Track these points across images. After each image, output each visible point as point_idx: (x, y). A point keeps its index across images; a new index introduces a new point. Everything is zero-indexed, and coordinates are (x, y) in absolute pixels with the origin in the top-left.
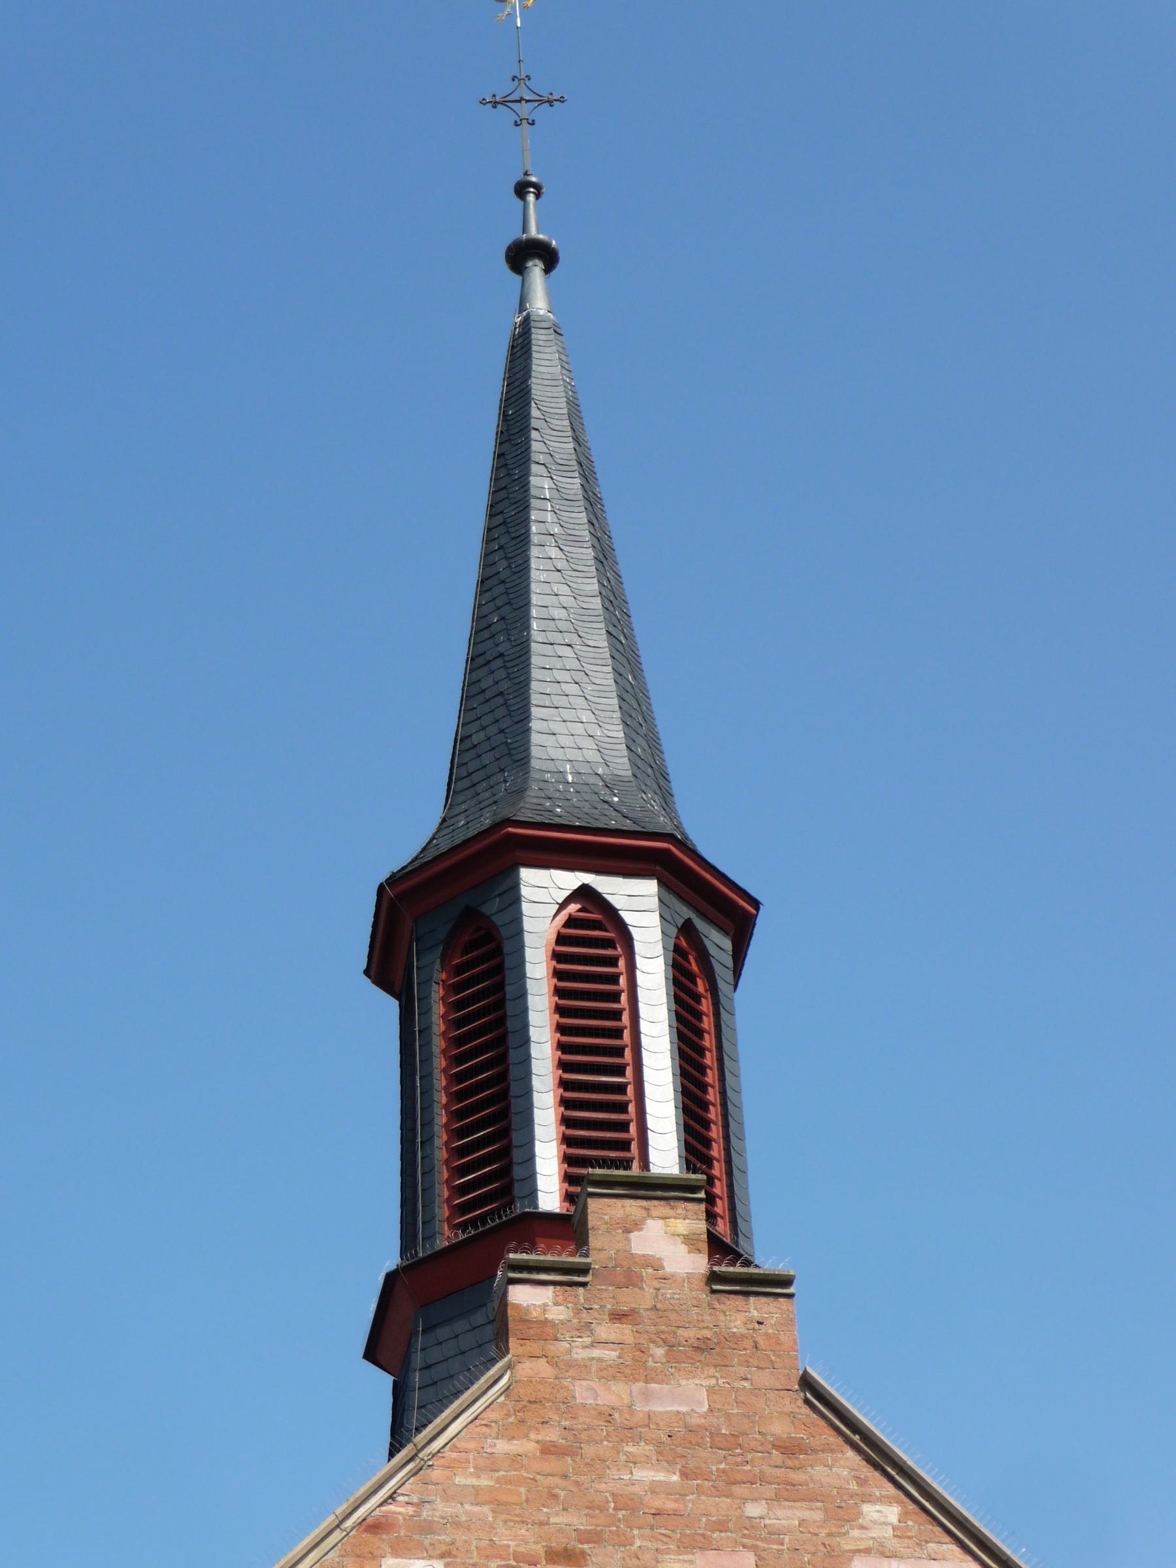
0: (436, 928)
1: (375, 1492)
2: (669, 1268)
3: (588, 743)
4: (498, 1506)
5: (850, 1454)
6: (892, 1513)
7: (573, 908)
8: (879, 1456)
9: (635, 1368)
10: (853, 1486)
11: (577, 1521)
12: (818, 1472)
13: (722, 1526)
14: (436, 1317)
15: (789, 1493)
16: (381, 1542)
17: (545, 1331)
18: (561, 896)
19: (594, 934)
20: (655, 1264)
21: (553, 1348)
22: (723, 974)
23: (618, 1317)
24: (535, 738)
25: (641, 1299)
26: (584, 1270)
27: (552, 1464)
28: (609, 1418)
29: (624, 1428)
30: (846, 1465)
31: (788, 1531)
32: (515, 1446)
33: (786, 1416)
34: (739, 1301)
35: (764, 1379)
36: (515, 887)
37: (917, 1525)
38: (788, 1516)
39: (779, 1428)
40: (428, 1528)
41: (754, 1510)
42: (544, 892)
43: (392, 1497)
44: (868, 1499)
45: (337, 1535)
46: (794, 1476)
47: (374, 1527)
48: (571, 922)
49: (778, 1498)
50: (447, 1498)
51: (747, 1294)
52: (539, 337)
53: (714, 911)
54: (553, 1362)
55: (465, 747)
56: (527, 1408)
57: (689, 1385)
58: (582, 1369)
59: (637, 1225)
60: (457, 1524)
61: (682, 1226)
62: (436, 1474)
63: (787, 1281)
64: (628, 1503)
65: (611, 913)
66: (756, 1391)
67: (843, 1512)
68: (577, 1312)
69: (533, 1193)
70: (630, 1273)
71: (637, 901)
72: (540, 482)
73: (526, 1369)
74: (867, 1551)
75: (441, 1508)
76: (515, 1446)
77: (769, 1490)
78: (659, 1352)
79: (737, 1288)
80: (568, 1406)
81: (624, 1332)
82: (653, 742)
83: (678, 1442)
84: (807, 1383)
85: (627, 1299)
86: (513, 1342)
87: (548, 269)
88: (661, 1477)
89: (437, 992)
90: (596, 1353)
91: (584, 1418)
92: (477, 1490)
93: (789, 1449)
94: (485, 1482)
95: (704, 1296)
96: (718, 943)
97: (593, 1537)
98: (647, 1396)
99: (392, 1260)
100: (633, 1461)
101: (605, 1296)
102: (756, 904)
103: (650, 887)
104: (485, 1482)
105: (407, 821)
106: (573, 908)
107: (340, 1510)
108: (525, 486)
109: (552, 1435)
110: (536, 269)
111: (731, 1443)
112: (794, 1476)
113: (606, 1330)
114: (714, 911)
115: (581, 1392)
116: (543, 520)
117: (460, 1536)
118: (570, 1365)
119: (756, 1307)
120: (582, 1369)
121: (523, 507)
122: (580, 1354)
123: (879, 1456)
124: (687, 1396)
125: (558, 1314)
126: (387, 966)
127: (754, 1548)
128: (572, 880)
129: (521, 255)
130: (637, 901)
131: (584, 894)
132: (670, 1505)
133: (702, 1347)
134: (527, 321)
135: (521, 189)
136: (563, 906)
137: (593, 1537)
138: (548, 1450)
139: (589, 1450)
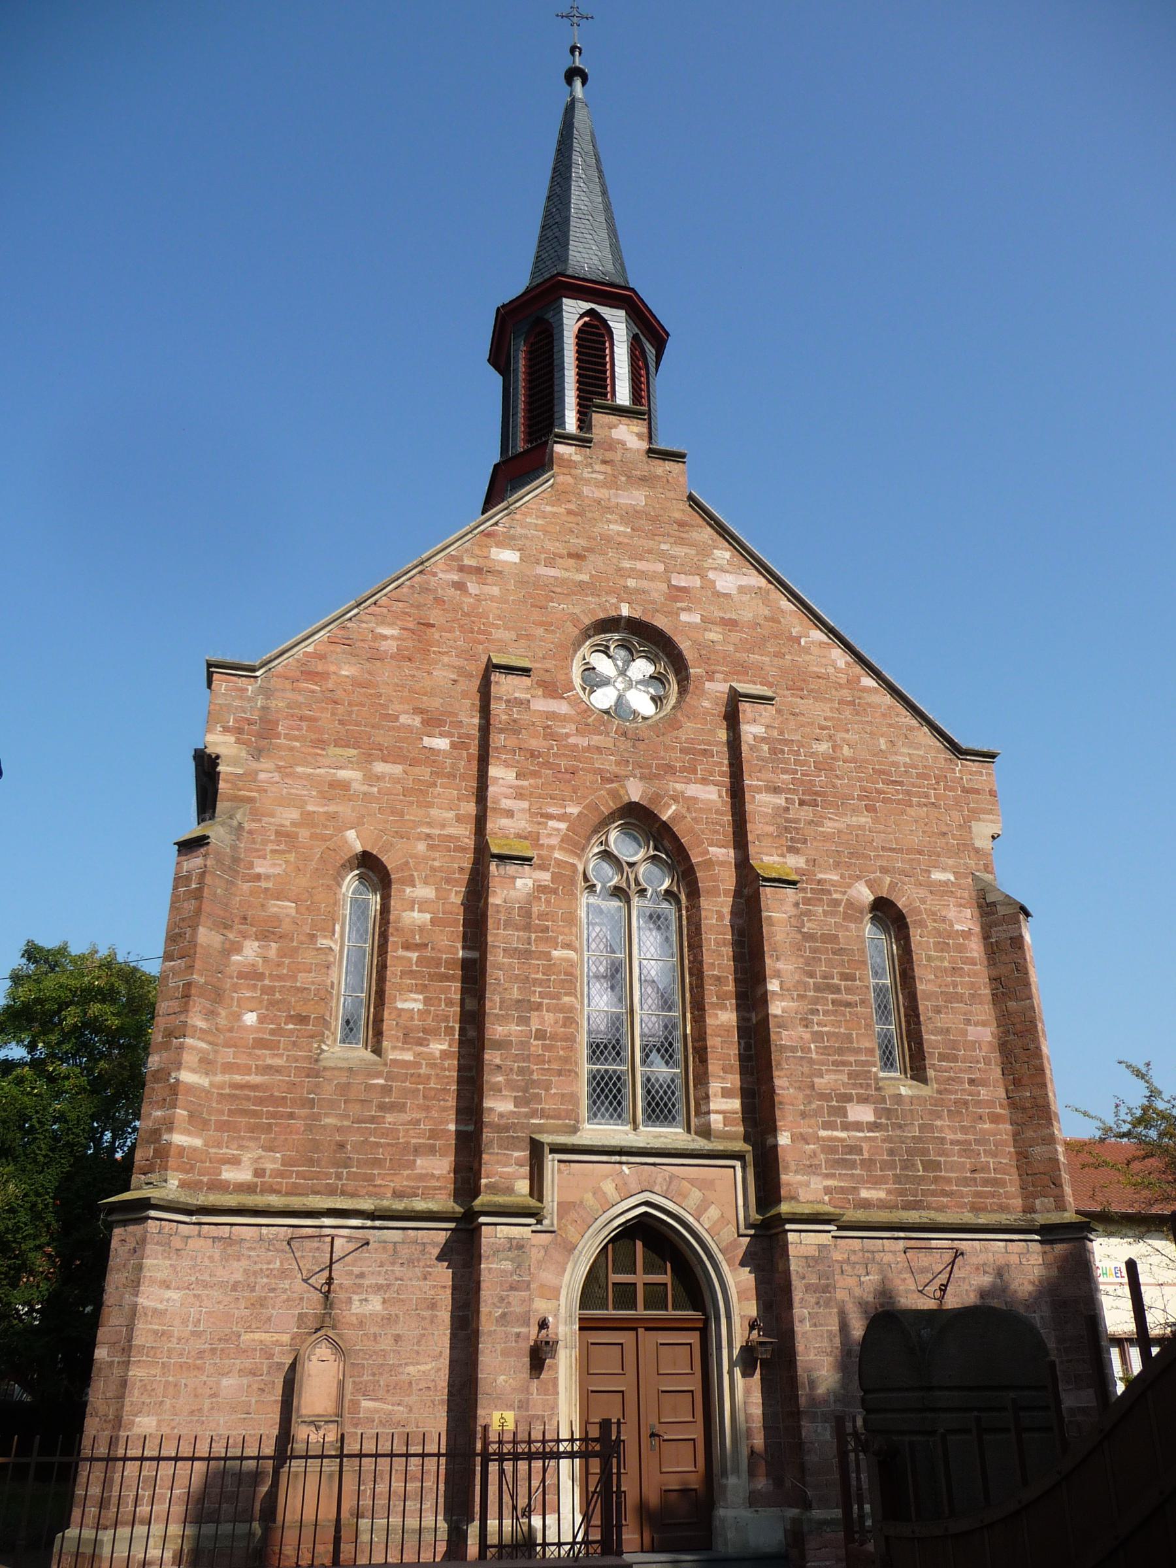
0: (522, 331)
1: (488, 520)
2: (629, 445)
3: (594, 257)
4: (546, 532)
5: (709, 529)
6: (727, 555)
7: (586, 319)
8: (722, 531)
9: (611, 483)
10: (710, 542)
11: (583, 542)
12: (695, 535)
13: (650, 552)
14: (522, 462)
15: (681, 542)
16: (490, 541)
17: (569, 464)
18: (582, 311)
19: (594, 337)
20: (623, 443)
21: (573, 471)
22: (652, 369)
23: (604, 462)
24: (571, 253)
25: (617, 456)
26: (590, 441)
27: (571, 518)
28: (599, 503)
29: (607, 508)
30: (707, 534)
31: (680, 557)
32: (555, 509)
33: (681, 511)
34: (660, 462)
35: (671, 494)
36: (561, 305)
37: (738, 560)
38: (680, 551)
39: (677, 515)
40: (513, 538)
41: (664, 547)
42: (573, 312)
43: (496, 524)
44: (717, 548)
45: (470, 536)
46: (683, 535)
47: (488, 535)
48: (585, 324)
49: (675, 543)
50: (522, 527)
51: (664, 460)
52: (578, 105)
53: (650, 334)
54: (574, 477)
55: (548, 214)
56: (560, 495)
57: (636, 493)
58: (587, 482)
59: (615, 427)
60: (526, 537)
61: (636, 429)
62: (517, 517)
63: (683, 456)
64: (607, 539)
65: (604, 322)
66: (667, 499)
67: (705, 551)
68: (586, 458)
69: (562, 425)
70: (611, 445)
71: (618, 323)
72: (577, 159)
73: (561, 479)
74: (715, 569)
75: (520, 531)
76: (555, 509)
77: (672, 540)
78: (623, 479)
79: (478, 1488)
80: (579, 495)
81: (608, 469)
82: (622, 265)
83: (630, 516)
84: (691, 498)
85: (609, 456)
86: (555, 467)
87: (584, 84)
88: (622, 529)
89: (522, 355)
90: (594, 476)
91: (587, 502)
92: (536, 525)
93: (682, 524)
94: (540, 522)
95: (645, 458)
96: (650, 351)
97: (590, 550)
98: (617, 496)
99: (497, 459)
100: (609, 521)
101: (597, 453)
102: (668, 335)
103: (622, 313)
104: (540, 522)
105: (515, 281)
106: (586, 319)
107: (473, 524)
108: (570, 158)
109: (572, 507)
110: (578, 83)
111: (655, 519)
112: (683, 535)
113: (598, 467)
114: (650, 334)
115: (586, 491)
116: (577, 172)
117: (528, 543)
118: (581, 479)
119: (669, 465)
120: (587, 482)
121: (569, 167)
122: (586, 475)
123: (722, 531)
124: (637, 498)
125: (577, 458)
126: (499, 358)
127: (664, 562)
128: (587, 306)
129: (573, 74)
130: (618, 323)
131: (591, 313)
132: (626, 541)
133: (643, 479)
134: (573, 101)
135: (573, 49)
136: (582, 316)
137: (590, 550)
138: (570, 512)
139: (589, 515)
